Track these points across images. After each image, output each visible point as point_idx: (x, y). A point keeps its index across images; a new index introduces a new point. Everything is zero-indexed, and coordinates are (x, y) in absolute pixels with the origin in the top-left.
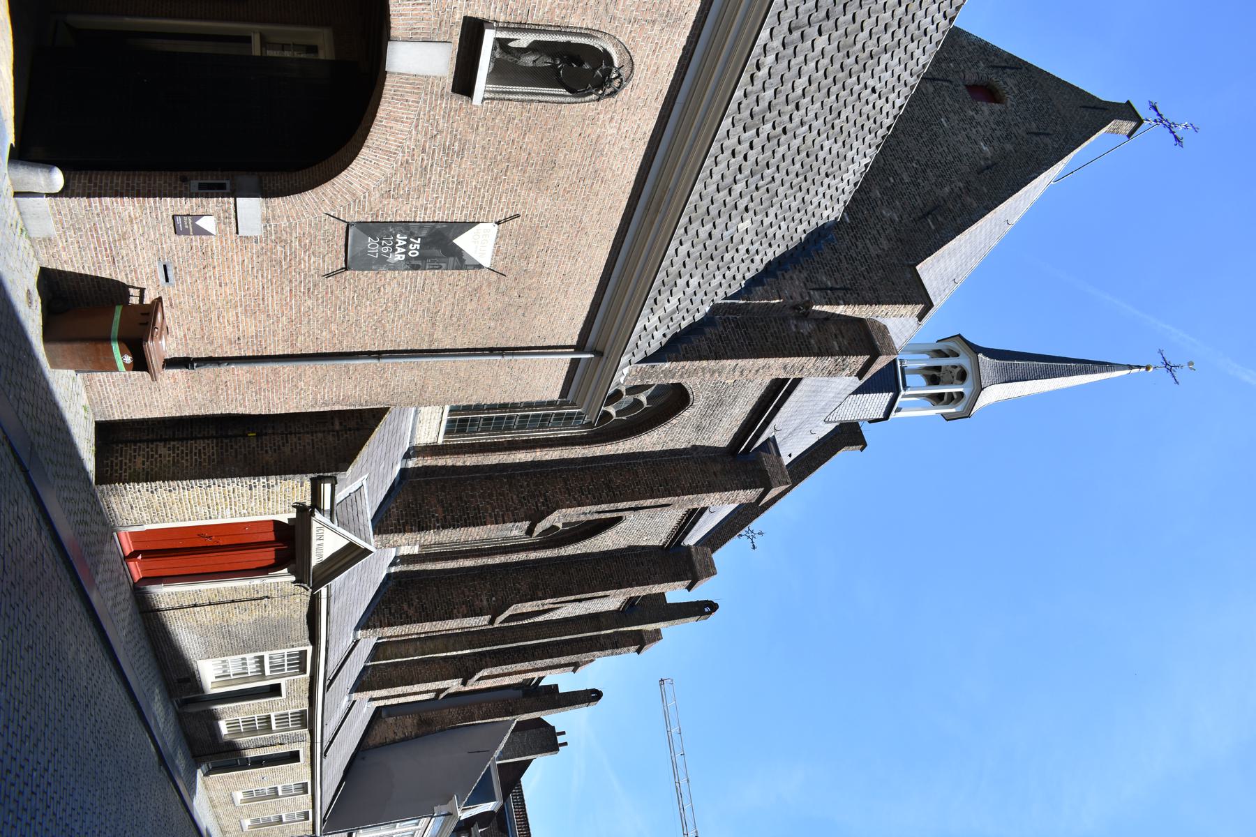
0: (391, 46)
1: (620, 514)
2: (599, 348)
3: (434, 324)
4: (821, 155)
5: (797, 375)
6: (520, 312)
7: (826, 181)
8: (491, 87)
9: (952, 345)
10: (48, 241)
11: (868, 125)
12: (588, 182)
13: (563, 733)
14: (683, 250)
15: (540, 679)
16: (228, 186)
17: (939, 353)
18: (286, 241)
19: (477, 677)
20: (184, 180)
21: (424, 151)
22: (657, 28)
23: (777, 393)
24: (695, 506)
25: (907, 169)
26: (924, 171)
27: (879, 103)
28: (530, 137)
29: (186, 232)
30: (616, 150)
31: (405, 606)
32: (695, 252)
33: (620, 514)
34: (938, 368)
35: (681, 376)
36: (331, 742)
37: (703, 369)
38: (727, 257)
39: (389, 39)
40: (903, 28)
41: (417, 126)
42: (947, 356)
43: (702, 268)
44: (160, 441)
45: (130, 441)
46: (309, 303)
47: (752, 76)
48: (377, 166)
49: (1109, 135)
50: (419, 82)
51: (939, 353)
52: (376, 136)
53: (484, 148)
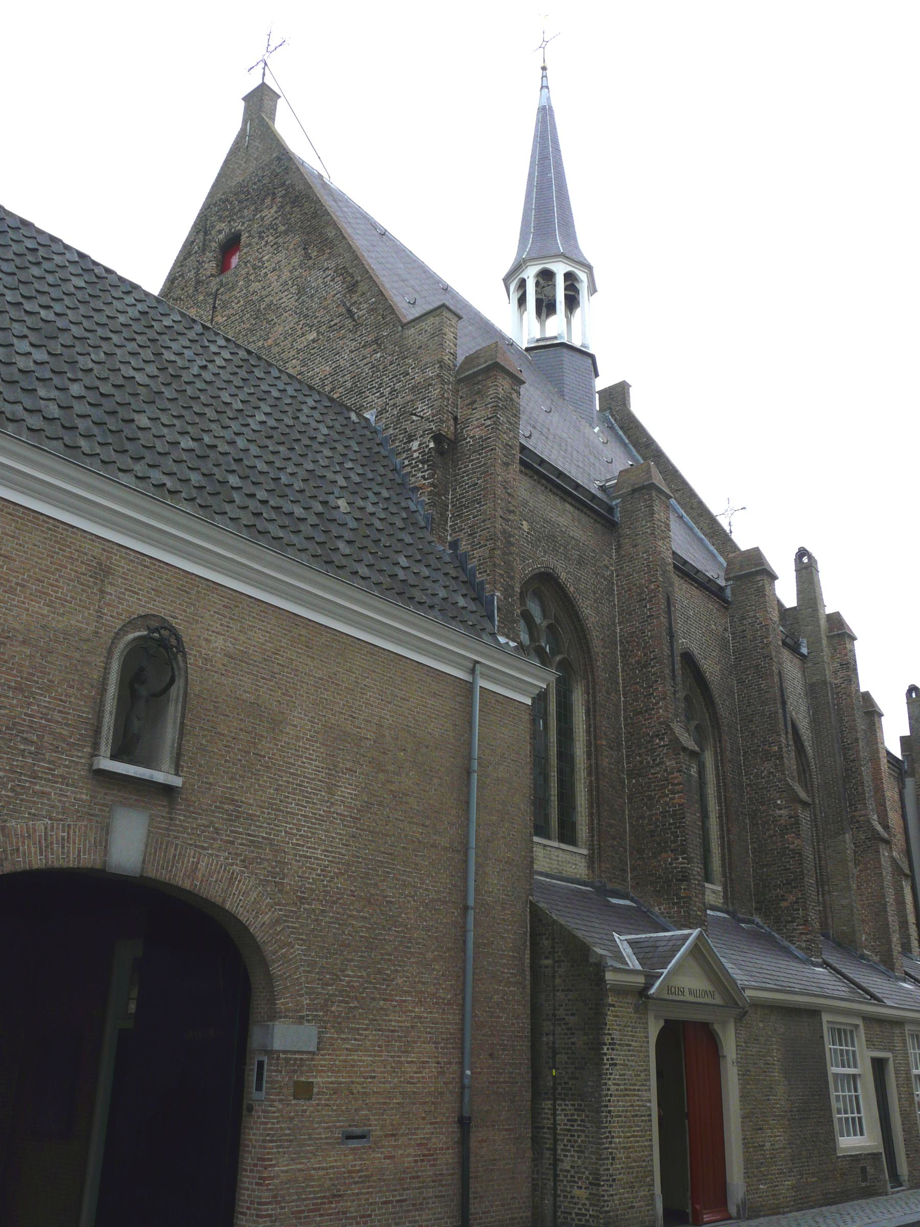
0: (111, 869)
4: (271, 422)
6: (424, 750)
7: (303, 419)
9: (512, 287)
11: (243, 373)
16: (261, 1059)
17: (522, 301)
18: (326, 1000)
20: (250, 1109)
22: (109, 589)
23: (534, 468)
24: (671, 568)
25: (303, 335)
26: (306, 316)
27: (219, 361)
30: (242, 637)
31: (784, 904)
32: (369, 559)
37: (504, 554)
38: (378, 525)
39: (104, 870)
40: (136, 336)
45: (555, 1201)
46: (400, 981)
48: (246, 894)
49: (285, 126)
50: (155, 842)
51: (522, 301)
52: (214, 892)
53: (232, 779)
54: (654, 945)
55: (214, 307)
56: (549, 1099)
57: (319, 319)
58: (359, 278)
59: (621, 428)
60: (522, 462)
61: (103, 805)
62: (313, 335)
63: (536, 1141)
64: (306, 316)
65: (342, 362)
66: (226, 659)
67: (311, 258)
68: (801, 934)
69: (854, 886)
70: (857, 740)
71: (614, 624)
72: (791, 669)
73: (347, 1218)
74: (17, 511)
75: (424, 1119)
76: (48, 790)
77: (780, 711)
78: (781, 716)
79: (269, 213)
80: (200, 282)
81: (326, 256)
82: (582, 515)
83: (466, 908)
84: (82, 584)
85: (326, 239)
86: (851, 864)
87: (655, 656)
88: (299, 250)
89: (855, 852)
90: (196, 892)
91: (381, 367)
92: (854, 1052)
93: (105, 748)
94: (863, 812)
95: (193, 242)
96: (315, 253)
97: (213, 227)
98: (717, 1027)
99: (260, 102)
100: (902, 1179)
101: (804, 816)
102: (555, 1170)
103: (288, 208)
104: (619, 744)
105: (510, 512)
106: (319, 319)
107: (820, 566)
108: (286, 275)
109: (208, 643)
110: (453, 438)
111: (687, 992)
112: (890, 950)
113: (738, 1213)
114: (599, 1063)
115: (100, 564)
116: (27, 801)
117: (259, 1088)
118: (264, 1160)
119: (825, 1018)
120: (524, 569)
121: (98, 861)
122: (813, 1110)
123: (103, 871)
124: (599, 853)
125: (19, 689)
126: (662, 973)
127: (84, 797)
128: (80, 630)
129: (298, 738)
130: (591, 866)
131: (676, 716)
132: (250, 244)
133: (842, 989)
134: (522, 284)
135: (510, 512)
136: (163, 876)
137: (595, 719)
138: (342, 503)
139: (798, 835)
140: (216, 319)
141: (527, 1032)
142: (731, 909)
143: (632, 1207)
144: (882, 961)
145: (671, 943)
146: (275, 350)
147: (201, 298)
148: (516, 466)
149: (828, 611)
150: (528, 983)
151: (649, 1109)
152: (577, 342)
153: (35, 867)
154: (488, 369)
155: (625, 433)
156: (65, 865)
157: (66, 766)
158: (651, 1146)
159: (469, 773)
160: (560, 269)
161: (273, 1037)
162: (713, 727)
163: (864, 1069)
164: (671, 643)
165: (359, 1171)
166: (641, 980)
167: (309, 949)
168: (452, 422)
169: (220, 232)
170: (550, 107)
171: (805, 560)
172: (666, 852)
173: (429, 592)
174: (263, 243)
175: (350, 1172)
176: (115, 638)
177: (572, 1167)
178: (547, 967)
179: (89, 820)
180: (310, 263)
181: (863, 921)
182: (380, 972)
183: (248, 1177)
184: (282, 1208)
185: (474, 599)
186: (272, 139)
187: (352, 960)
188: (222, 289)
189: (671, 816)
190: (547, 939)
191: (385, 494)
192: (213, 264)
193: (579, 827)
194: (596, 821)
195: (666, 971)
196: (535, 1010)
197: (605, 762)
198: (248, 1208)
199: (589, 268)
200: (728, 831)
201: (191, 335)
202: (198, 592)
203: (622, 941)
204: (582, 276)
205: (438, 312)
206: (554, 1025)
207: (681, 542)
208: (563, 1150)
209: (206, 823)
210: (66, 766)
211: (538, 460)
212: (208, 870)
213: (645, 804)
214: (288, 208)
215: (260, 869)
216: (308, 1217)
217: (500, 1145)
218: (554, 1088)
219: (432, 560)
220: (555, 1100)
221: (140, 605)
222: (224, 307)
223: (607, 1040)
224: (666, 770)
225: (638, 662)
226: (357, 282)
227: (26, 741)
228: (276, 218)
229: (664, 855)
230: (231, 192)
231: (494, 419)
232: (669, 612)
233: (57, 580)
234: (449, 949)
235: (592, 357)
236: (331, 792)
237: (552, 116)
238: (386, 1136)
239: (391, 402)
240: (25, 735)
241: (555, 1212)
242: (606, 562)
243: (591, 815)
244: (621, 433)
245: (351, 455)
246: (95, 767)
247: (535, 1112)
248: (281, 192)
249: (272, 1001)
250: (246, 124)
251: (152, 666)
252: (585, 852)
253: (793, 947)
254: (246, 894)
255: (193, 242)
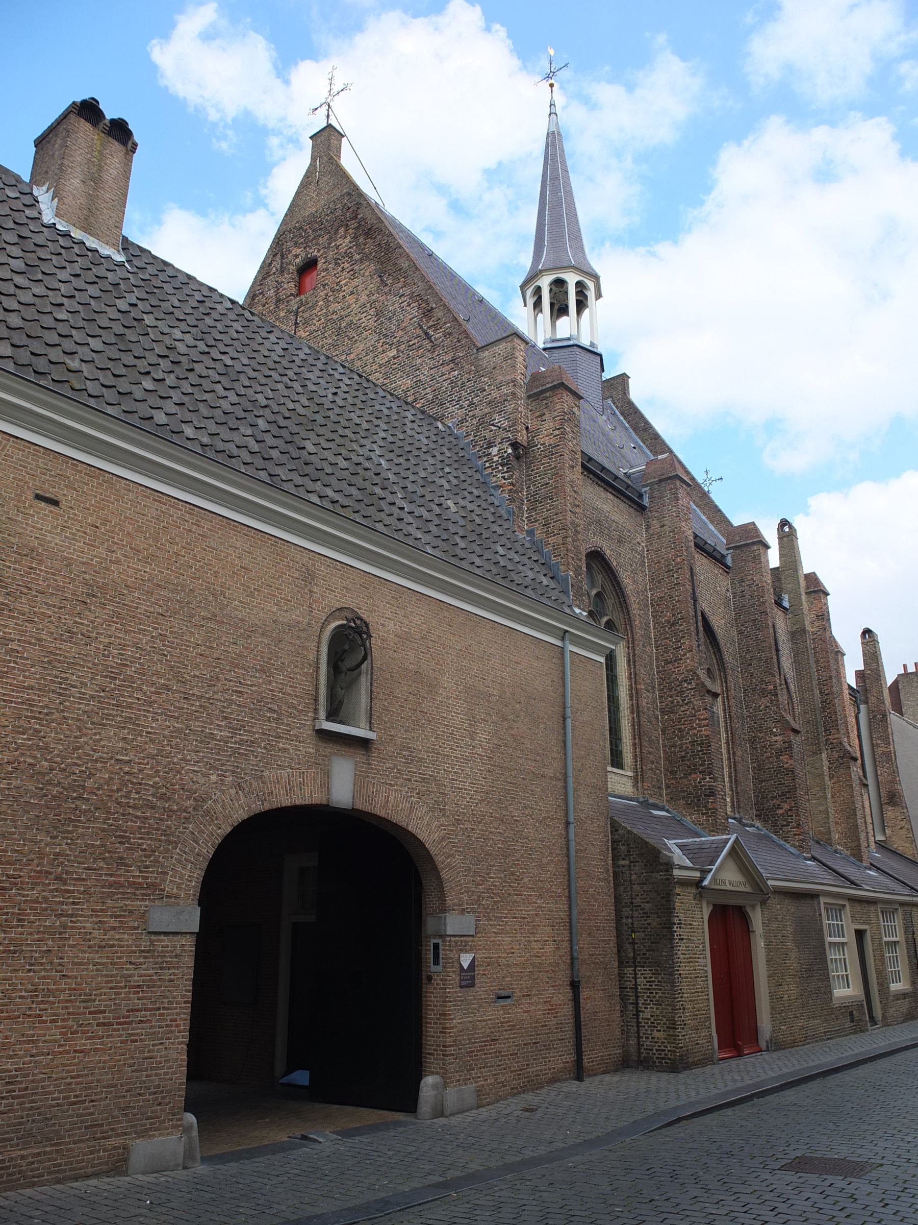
1: (699, 613)
2: (562, 634)
3: (542, 776)
5: (579, 456)
6: (533, 702)
7: (409, 432)
8: (363, 724)
9: (529, 292)
10: (479, 1092)
12: (431, 644)
13: (905, 666)
14: (478, 561)
15: (850, 687)
16: (436, 941)
17: (538, 305)
19: (849, 748)
20: (430, 978)
21: (410, 780)
23: (593, 471)
24: (692, 544)
26: (386, 336)
28: (397, 693)
29: (473, 978)
30: (406, 621)
31: (780, 811)
32: (478, 550)
33: (699, 613)
34: (552, 305)
35: (580, 560)
36: (912, 888)
37: (574, 541)
41: (391, 785)
42: (540, 298)
43: (488, 543)
44: (637, 1015)
45: (638, 1041)
46: (526, 880)
47: (343, 507)
48: (421, 818)
51: (538, 305)
52: (399, 819)
54: (701, 848)
55: (296, 323)
56: (630, 966)
57: (398, 339)
58: (434, 306)
59: (622, 414)
60: (584, 466)
61: (325, 756)
62: (394, 352)
63: (623, 998)
64: (386, 336)
65: (422, 377)
66: (397, 639)
67: (387, 285)
68: (795, 835)
69: (829, 796)
70: (831, 677)
71: (646, 590)
72: (782, 624)
73: (502, 1056)
74: (250, 532)
75: (547, 983)
76: (287, 746)
77: (775, 657)
78: (775, 660)
79: (345, 243)
80: (280, 300)
81: (400, 285)
82: (619, 501)
83: (568, 824)
84: (297, 586)
85: (400, 270)
86: (827, 778)
87: (700, 620)
88: (375, 277)
89: (830, 768)
90: (389, 818)
91: (459, 383)
92: (842, 925)
93: (322, 714)
94: (836, 736)
95: (270, 264)
96: (390, 281)
97: (290, 252)
98: (748, 909)
99: (327, 140)
100: (876, 1019)
101: (796, 740)
102: (638, 1019)
103: (361, 240)
104: (654, 687)
105: (577, 506)
106: (398, 339)
107: (799, 535)
108: (364, 298)
109: (385, 627)
110: (525, 444)
111: (727, 883)
112: (859, 846)
113: (767, 1047)
114: (672, 939)
115: (307, 570)
116: (276, 756)
117: (436, 962)
118: (446, 1015)
119: (823, 900)
120: (585, 548)
121: (324, 799)
122: (816, 970)
123: (328, 805)
124: (642, 775)
125: (262, 671)
126: (711, 870)
127: (311, 750)
128: (298, 622)
129: (448, 698)
130: (635, 785)
131: (700, 664)
132: (327, 269)
133: (829, 878)
134: (538, 290)
135: (577, 506)
136: (367, 808)
137: (635, 668)
138: (450, 503)
139: (791, 757)
140: (298, 334)
141: (613, 916)
142: (737, 816)
143: (698, 1044)
144: (852, 855)
145: (714, 846)
146: (358, 364)
147: (282, 314)
148: (579, 468)
149: (806, 570)
150: (611, 879)
151: (706, 971)
152: (585, 342)
153: (284, 805)
154: (554, 388)
155: (625, 418)
156: (304, 803)
157: (298, 728)
158: (708, 999)
159: (564, 719)
160: (571, 279)
161: (445, 925)
162: (719, 670)
163: (849, 938)
164: (695, 605)
165: (508, 1022)
166: (698, 874)
167: (465, 859)
168: (525, 432)
169: (296, 256)
170: (559, 134)
171: (786, 529)
172: (695, 773)
173: (523, 574)
174: (340, 269)
175: (502, 1023)
176: (322, 627)
177: (652, 1016)
178: (624, 866)
179: (317, 768)
180: (386, 289)
181: (837, 823)
182: (513, 874)
183: (433, 1028)
184: (460, 1049)
185: (552, 578)
186: (342, 176)
187: (494, 866)
188: (302, 308)
189: (699, 745)
190: (623, 845)
191: (476, 492)
192: (292, 285)
193: (624, 755)
194: (638, 750)
195: (714, 868)
196: (617, 899)
197: (644, 702)
198: (436, 1050)
199: (596, 278)
200: (734, 754)
201: (320, 365)
202: (374, 587)
203: (670, 843)
204: (591, 284)
205: (510, 339)
206: (632, 910)
207: (699, 524)
208: (643, 1004)
209: (392, 766)
210: (298, 728)
211: (587, 459)
212: (394, 803)
213: (677, 735)
214: (361, 240)
215: (429, 799)
216: (476, 1056)
217: (598, 1000)
218: (634, 958)
219: (518, 546)
220: (636, 967)
221: (337, 600)
222: (306, 322)
223: (676, 920)
224: (693, 709)
225: (668, 621)
226: (432, 309)
227: (271, 710)
228: (351, 248)
229: (693, 776)
230: (304, 221)
231: (562, 430)
232: (692, 581)
233: (281, 585)
234: (557, 855)
235: (601, 356)
236: (473, 739)
237: (561, 141)
238: (524, 996)
239: (471, 414)
240: (269, 706)
241: (639, 1049)
242: (638, 540)
243: (634, 745)
244: (622, 418)
245: (447, 461)
246: (317, 728)
247: (621, 976)
248: (353, 224)
249: (442, 898)
250: (315, 161)
251: (349, 647)
252: (631, 774)
253: (788, 846)
254: (421, 818)
255: (270, 264)
